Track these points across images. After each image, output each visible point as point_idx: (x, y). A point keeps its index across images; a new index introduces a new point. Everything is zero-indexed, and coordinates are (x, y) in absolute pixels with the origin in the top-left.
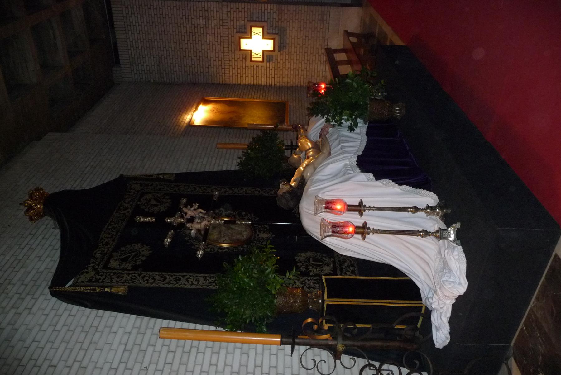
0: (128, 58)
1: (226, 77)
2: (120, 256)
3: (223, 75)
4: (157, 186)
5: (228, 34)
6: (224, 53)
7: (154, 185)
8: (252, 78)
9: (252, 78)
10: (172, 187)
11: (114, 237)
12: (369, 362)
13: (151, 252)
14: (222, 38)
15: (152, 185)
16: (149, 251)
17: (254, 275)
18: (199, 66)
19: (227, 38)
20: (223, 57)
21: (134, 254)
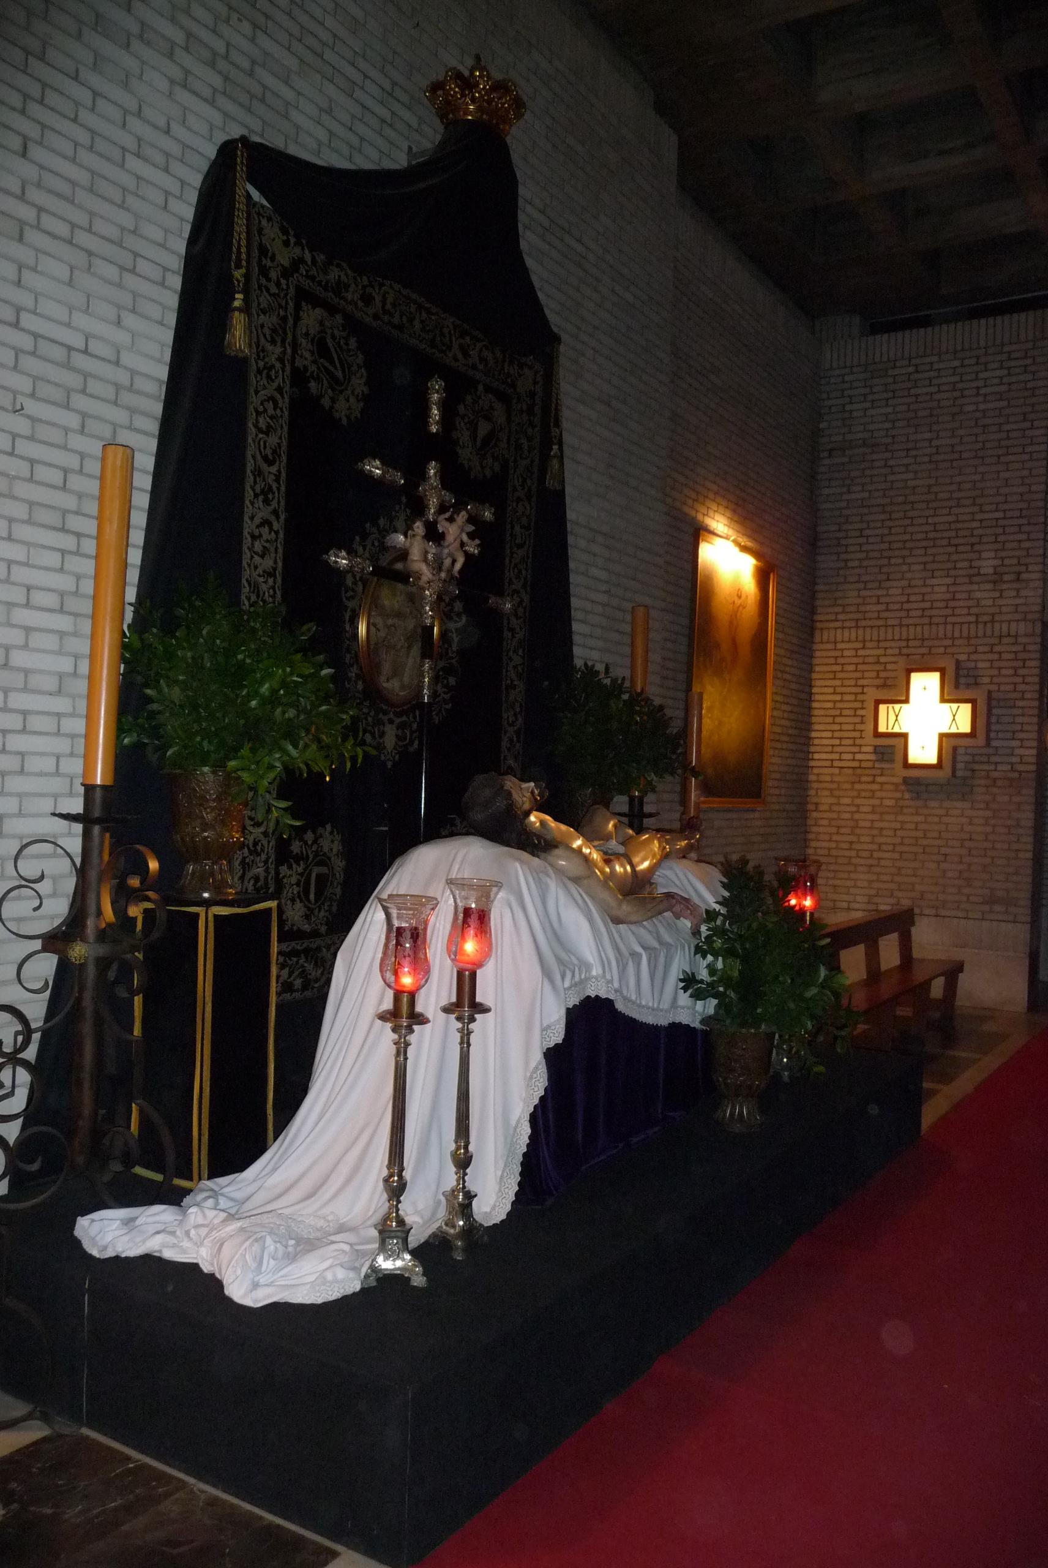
1: (832, 633)
3: (839, 624)
4: (530, 439)
6: (857, 627)
7: (530, 431)
8: (830, 705)
9: (830, 705)
10: (524, 481)
13: (345, 421)
21: (339, 374)
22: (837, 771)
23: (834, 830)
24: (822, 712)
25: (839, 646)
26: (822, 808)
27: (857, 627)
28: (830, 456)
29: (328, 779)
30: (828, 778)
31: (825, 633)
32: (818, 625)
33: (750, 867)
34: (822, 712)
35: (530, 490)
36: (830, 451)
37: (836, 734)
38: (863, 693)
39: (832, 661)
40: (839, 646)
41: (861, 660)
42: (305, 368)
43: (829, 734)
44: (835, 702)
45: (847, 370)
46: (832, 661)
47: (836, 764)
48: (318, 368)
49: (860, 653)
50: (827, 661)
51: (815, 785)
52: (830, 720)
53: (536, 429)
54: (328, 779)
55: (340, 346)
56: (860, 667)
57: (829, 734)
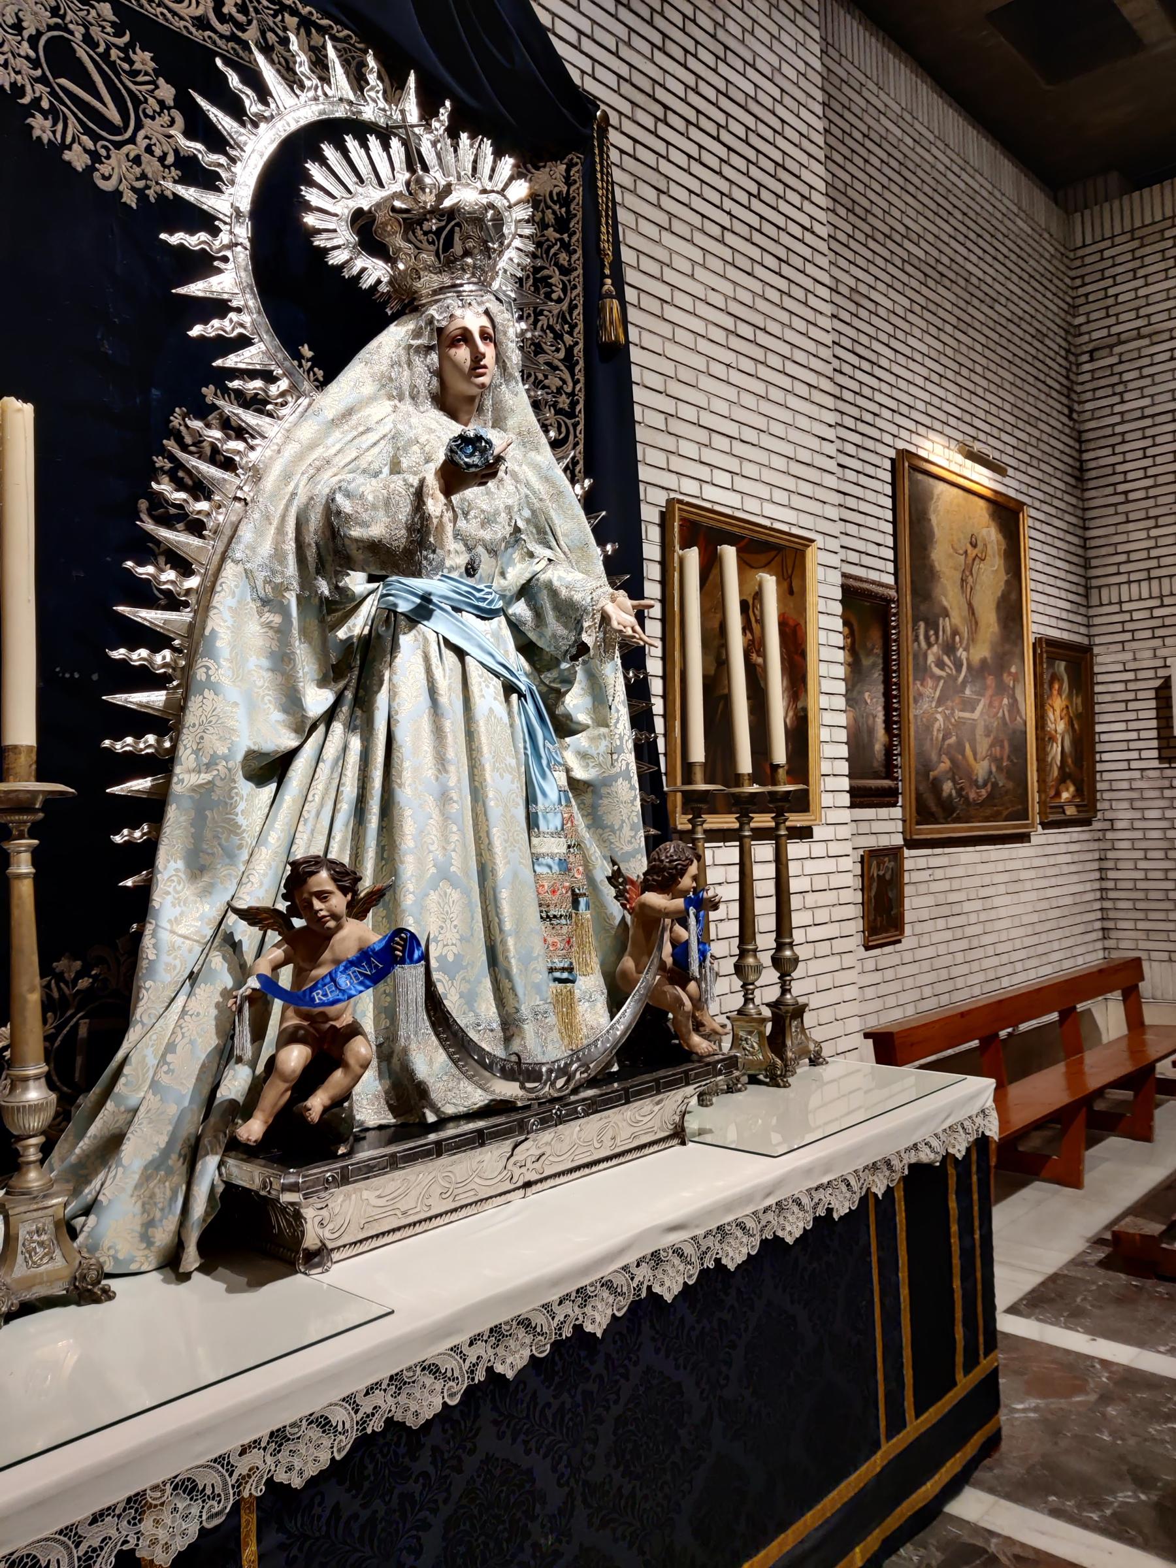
0: (1158, 218)
1: (1115, 590)
2: (88, 40)
3: (1124, 578)
4: (565, 271)
5: (1120, 603)
6: (1150, 579)
7: (563, 258)
8: (1121, 687)
9: (1121, 687)
10: (558, 336)
11: (225, 29)
12: (609, 295)
13: (130, 199)
14: (1144, 575)
15: (566, 246)
16: (140, 193)
17: (168, 659)
18: (1149, 482)
19: (1145, 595)
20: (1133, 577)
21: (113, 114)
22: (1137, 774)
23: (1140, 854)
24: (1108, 698)
25: (1126, 607)
26: (1119, 825)
27: (1150, 579)
28: (1092, 360)
29: (129, 883)
30: (1125, 785)
31: (1105, 592)
32: (1095, 583)
33: (519, 274)
34: (1108, 698)
35: (569, 350)
36: (1091, 352)
37: (1132, 725)
38: (1165, 666)
39: (1119, 628)
40: (1126, 607)
41: (1158, 622)
42: (19, 91)
43: (1122, 726)
44: (1126, 682)
45: (1108, 243)
46: (1119, 628)
47: (1134, 765)
48: (53, 93)
49: (1156, 613)
50: (1113, 688)
51: (1107, 796)
52: (1122, 706)
53: (575, 256)
54: (129, 883)
55: (112, 65)
56: (1158, 632)
57: (1122, 726)
